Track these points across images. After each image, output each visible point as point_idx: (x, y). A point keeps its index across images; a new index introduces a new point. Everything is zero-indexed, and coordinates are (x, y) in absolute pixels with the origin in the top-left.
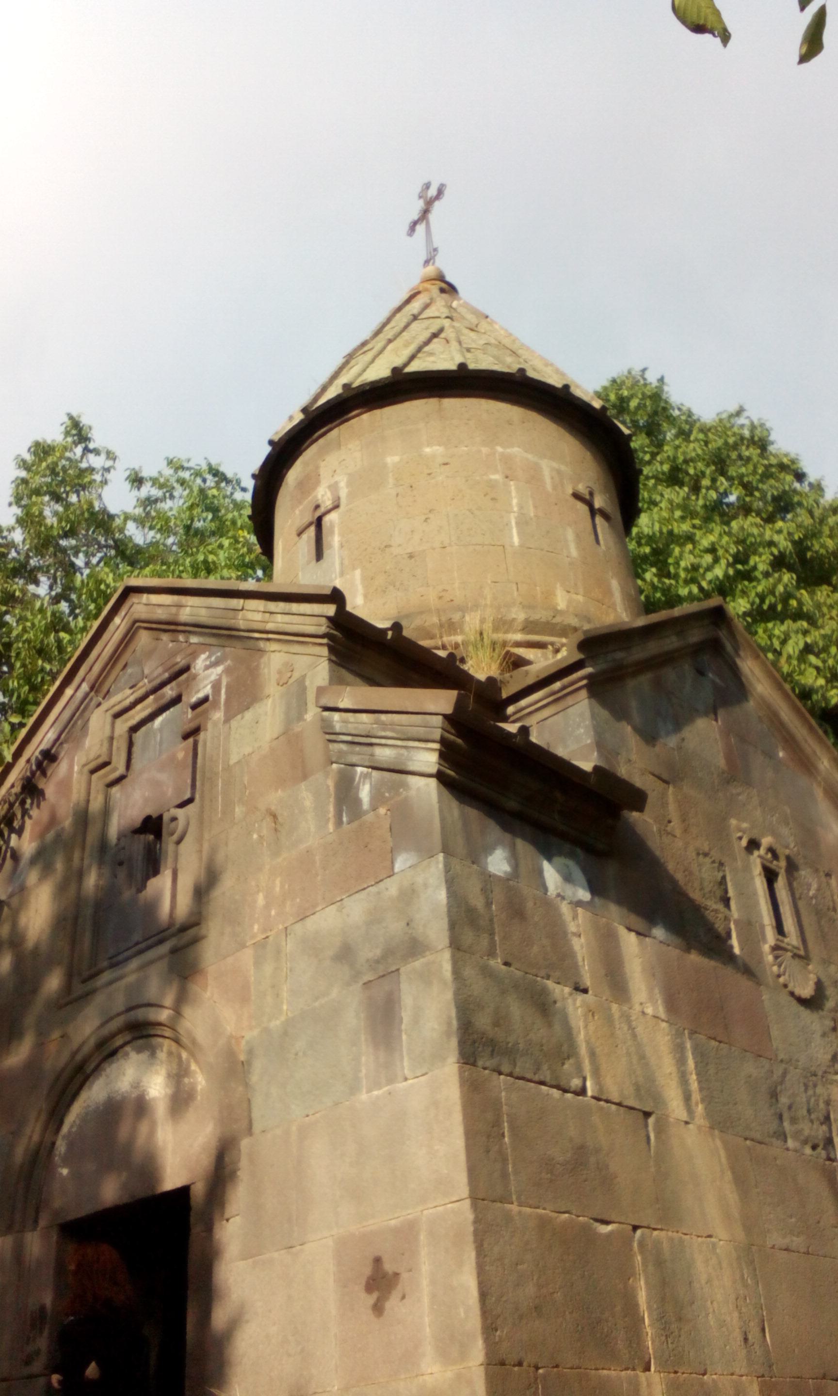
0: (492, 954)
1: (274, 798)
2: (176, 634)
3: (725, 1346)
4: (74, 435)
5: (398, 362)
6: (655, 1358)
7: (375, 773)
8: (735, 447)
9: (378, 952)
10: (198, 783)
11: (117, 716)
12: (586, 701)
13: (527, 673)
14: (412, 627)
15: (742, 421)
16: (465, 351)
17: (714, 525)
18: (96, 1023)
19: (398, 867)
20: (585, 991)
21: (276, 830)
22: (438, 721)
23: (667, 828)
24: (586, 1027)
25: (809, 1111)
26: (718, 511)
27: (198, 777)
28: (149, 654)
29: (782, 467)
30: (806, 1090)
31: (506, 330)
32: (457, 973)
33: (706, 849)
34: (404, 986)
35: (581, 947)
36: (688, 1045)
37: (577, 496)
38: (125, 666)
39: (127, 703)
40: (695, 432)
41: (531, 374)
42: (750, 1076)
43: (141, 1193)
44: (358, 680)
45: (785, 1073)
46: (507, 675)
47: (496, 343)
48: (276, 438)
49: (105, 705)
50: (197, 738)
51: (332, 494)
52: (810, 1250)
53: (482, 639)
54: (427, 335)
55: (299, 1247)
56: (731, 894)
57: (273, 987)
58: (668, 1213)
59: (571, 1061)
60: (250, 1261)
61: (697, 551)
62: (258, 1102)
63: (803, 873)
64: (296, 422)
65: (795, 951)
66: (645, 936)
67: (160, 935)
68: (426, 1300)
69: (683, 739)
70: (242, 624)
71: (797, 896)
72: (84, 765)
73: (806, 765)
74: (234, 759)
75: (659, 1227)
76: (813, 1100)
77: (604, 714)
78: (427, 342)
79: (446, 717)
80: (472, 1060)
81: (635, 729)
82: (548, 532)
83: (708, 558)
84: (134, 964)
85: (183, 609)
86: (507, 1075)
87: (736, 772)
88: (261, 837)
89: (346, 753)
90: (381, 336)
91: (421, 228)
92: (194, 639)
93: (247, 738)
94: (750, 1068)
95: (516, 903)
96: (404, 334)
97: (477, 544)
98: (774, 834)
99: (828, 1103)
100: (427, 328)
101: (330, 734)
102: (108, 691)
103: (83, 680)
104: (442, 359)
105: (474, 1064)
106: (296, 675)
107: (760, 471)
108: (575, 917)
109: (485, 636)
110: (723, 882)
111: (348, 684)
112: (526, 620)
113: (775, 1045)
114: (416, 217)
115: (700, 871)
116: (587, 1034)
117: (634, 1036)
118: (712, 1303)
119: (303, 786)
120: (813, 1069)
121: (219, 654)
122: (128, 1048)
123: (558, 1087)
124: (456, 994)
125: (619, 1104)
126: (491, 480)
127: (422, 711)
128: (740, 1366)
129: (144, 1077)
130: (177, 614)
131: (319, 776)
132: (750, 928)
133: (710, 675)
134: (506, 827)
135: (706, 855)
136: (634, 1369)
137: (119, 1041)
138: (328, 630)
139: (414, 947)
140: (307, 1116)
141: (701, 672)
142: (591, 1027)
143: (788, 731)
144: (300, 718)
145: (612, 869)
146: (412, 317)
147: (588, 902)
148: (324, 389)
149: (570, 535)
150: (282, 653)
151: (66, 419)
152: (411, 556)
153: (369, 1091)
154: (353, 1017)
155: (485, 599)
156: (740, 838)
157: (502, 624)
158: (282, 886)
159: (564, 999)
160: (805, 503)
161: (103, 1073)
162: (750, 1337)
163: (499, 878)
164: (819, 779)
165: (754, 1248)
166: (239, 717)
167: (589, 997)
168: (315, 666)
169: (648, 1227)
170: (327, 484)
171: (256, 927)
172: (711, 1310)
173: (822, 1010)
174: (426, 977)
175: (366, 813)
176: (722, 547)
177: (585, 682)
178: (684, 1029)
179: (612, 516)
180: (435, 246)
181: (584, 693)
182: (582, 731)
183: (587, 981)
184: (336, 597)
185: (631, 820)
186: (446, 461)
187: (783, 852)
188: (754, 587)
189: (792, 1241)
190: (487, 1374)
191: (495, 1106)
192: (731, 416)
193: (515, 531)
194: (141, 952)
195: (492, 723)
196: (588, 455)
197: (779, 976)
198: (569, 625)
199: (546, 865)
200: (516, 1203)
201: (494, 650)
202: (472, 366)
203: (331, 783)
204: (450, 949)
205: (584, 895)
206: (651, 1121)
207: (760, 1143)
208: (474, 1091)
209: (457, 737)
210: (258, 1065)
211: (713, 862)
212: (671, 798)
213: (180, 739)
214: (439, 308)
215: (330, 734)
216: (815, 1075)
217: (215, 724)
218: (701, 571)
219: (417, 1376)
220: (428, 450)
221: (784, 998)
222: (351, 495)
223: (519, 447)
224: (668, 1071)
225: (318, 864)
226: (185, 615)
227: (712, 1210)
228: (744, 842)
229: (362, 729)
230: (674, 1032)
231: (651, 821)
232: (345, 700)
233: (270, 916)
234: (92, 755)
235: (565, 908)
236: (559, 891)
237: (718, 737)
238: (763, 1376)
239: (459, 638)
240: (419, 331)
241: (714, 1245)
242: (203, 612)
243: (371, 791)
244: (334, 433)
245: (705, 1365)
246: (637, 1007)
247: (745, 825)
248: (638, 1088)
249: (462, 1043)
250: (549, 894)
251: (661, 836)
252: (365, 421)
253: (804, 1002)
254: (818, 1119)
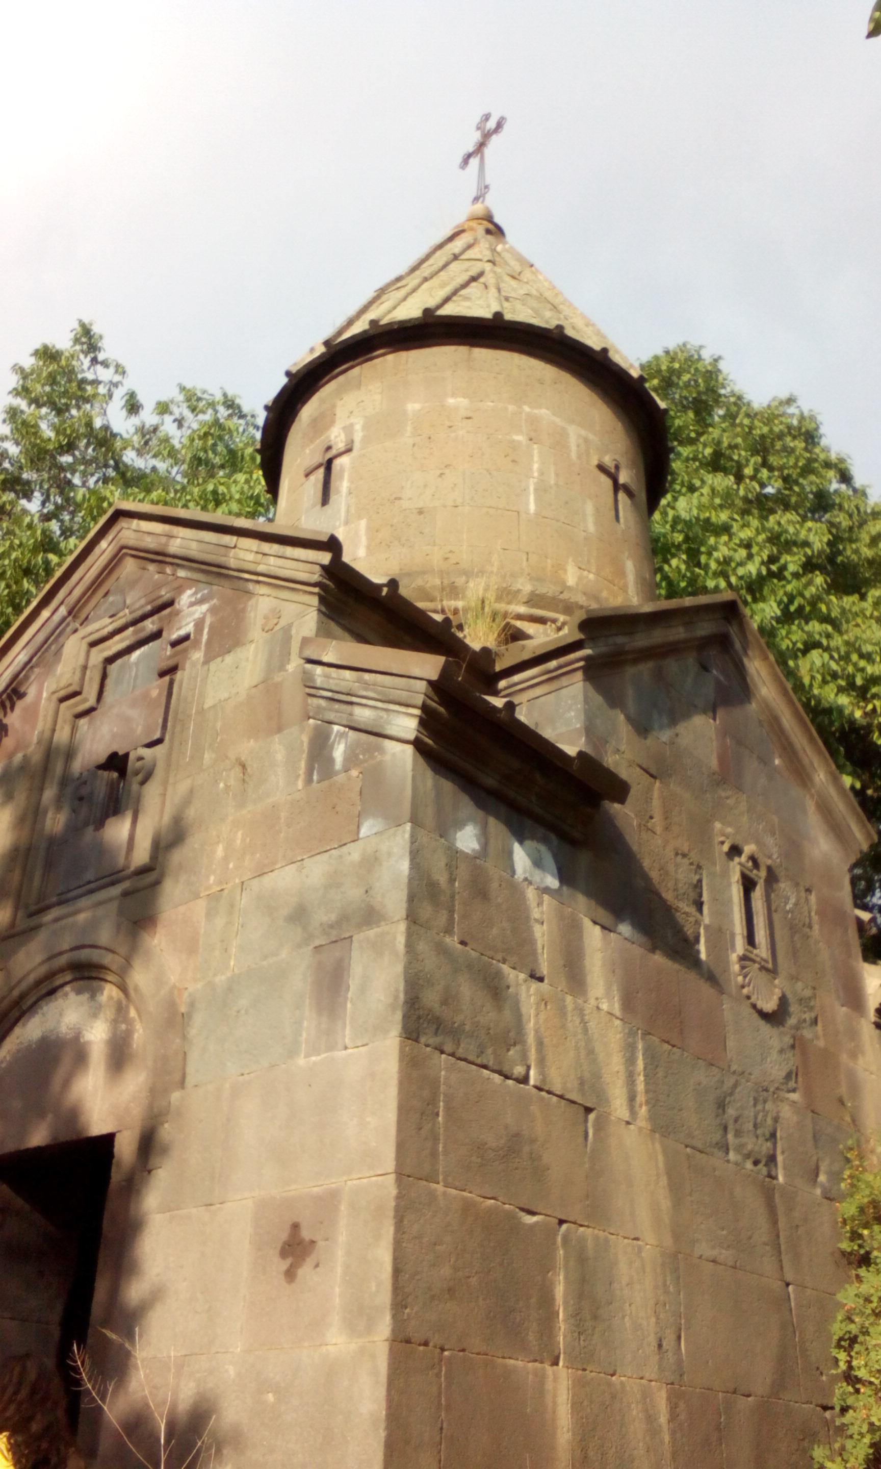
0: (449, 931)
1: (246, 748)
2: (162, 565)
3: (638, 1350)
4: (83, 344)
5: (431, 303)
6: (565, 1353)
7: (352, 733)
8: (780, 436)
9: (333, 917)
10: (169, 724)
11: (93, 644)
12: (581, 684)
13: (523, 647)
14: (413, 586)
15: (791, 410)
16: (503, 299)
17: (751, 518)
18: (39, 959)
19: (364, 832)
20: (541, 979)
21: (244, 780)
22: (422, 686)
23: (648, 824)
24: (537, 1015)
25: (756, 1126)
26: (762, 505)
27: (170, 718)
28: (133, 584)
29: (828, 465)
30: (755, 1105)
31: (550, 282)
32: (410, 947)
33: (686, 851)
34: (355, 954)
35: (543, 934)
36: (640, 1046)
37: (601, 468)
38: (107, 594)
39: (105, 632)
40: (741, 416)
41: (569, 332)
42: (699, 1084)
43: (64, 1137)
44: (347, 635)
45: (735, 1085)
46: (503, 648)
47: (538, 295)
48: (294, 370)
49: (82, 632)
50: (173, 677)
51: (346, 436)
52: (738, 1264)
53: (483, 608)
54: (465, 277)
55: (218, 1206)
56: (705, 898)
57: (222, 941)
58: (597, 1211)
59: (518, 1047)
60: (168, 1214)
61: (732, 545)
62: (194, 1056)
63: (782, 885)
64: (317, 354)
65: (763, 963)
66: (611, 931)
67: (113, 877)
68: (339, 1270)
69: (677, 735)
70: (232, 563)
71: (773, 908)
72: (54, 693)
73: (801, 775)
74: (209, 703)
75: (586, 1224)
76: (761, 1114)
77: (599, 699)
78: (465, 286)
79: (430, 682)
80: (414, 1036)
81: (628, 718)
82: (567, 503)
83: (743, 553)
84: (84, 902)
85: (172, 540)
86: (449, 1055)
87: (728, 775)
88: (227, 787)
89: (324, 709)
90: (417, 273)
91: (474, 162)
92: (181, 573)
93: (224, 683)
94: (702, 1076)
95: (480, 883)
96: (442, 273)
97: (490, 507)
98: (758, 842)
99: (776, 1120)
100: (467, 270)
101: (310, 688)
102: (87, 618)
103: (62, 603)
104: (477, 305)
105: (417, 1040)
106: (283, 623)
107: (800, 464)
108: (540, 904)
109: (487, 603)
110: (699, 884)
111: (335, 638)
112: (532, 593)
113: (729, 1055)
114: (471, 150)
115: (676, 872)
116: (537, 1023)
117: (586, 1030)
118: (630, 1305)
119: (276, 738)
120: (765, 1084)
121: (206, 591)
122: (67, 988)
123: (500, 1073)
124: (407, 968)
125: (561, 1097)
126: (514, 441)
127: (389, 671)
128: (651, 1371)
129: (74, 1016)
130: (166, 545)
131: (295, 730)
132: (720, 936)
133: (715, 672)
134: (481, 804)
135: (684, 856)
136: (542, 1362)
137: (59, 981)
138: (320, 579)
139: (370, 916)
140: (242, 1075)
141: (705, 668)
142: (542, 1016)
143: (787, 738)
144: (282, 667)
145: (584, 858)
146: (452, 256)
147: (555, 891)
148: (350, 323)
149: (589, 508)
150: (271, 598)
151: (76, 325)
152: (421, 512)
153: (307, 1056)
154: (300, 979)
155: (493, 565)
156: (723, 843)
157: (506, 594)
158: (243, 840)
159: (518, 985)
160: (846, 506)
161: (39, 1011)
162: (664, 1344)
163: (466, 855)
164: (813, 791)
165: (680, 1256)
166: (219, 659)
167: (545, 986)
168: (303, 615)
169: (574, 1223)
170: (342, 426)
171: (212, 878)
172: (628, 1312)
173: (783, 1026)
174: (378, 948)
175: (337, 773)
176: (757, 544)
177: (582, 664)
178: (638, 1029)
179: (636, 493)
180: (487, 183)
181: (579, 675)
182: (573, 714)
183: (544, 969)
184: (333, 545)
185: (612, 812)
186: (469, 415)
187: (764, 861)
188: (784, 586)
189: (721, 1254)
190: (391, 1349)
191: (434, 1084)
192: (781, 403)
193: (532, 498)
194: (91, 892)
195: (478, 694)
196: (619, 426)
197: (743, 987)
198: (576, 603)
199: (517, 847)
200: (441, 1184)
201: (494, 620)
202: (508, 316)
203: (305, 739)
204: (406, 922)
205: (552, 882)
206: (592, 1116)
207: (701, 1152)
208: (413, 1069)
209: (440, 704)
210: (198, 1019)
211: (691, 864)
212: (656, 794)
213: (156, 676)
214: (482, 250)
215: (310, 688)
216: (766, 1090)
217: (194, 665)
218: (733, 565)
219: (321, 1345)
220: (451, 401)
221: (747, 1011)
222: (366, 440)
223: (547, 409)
224: (616, 1069)
225: (282, 820)
226: (175, 547)
227: (644, 1216)
228: (726, 848)
229: (343, 686)
230: (627, 1031)
231: (633, 815)
232: (330, 654)
233: (228, 868)
234: (63, 683)
235: (531, 894)
236: (527, 875)
237: (714, 737)
238: (672, 1384)
239: (460, 604)
240: (458, 273)
241: (640, 1249)
242: (194, 545)
243: (345, 751)
244: (357, 370)
245: (616, 1366)
246: (593, 1002)
247: (729, 830)
248: (582, 1083)
249: (406, 1017)
250: (516, 877)
251: (640, 831)
252: (389, 363)
253: (765, 1016)
254: (764, 1135)
